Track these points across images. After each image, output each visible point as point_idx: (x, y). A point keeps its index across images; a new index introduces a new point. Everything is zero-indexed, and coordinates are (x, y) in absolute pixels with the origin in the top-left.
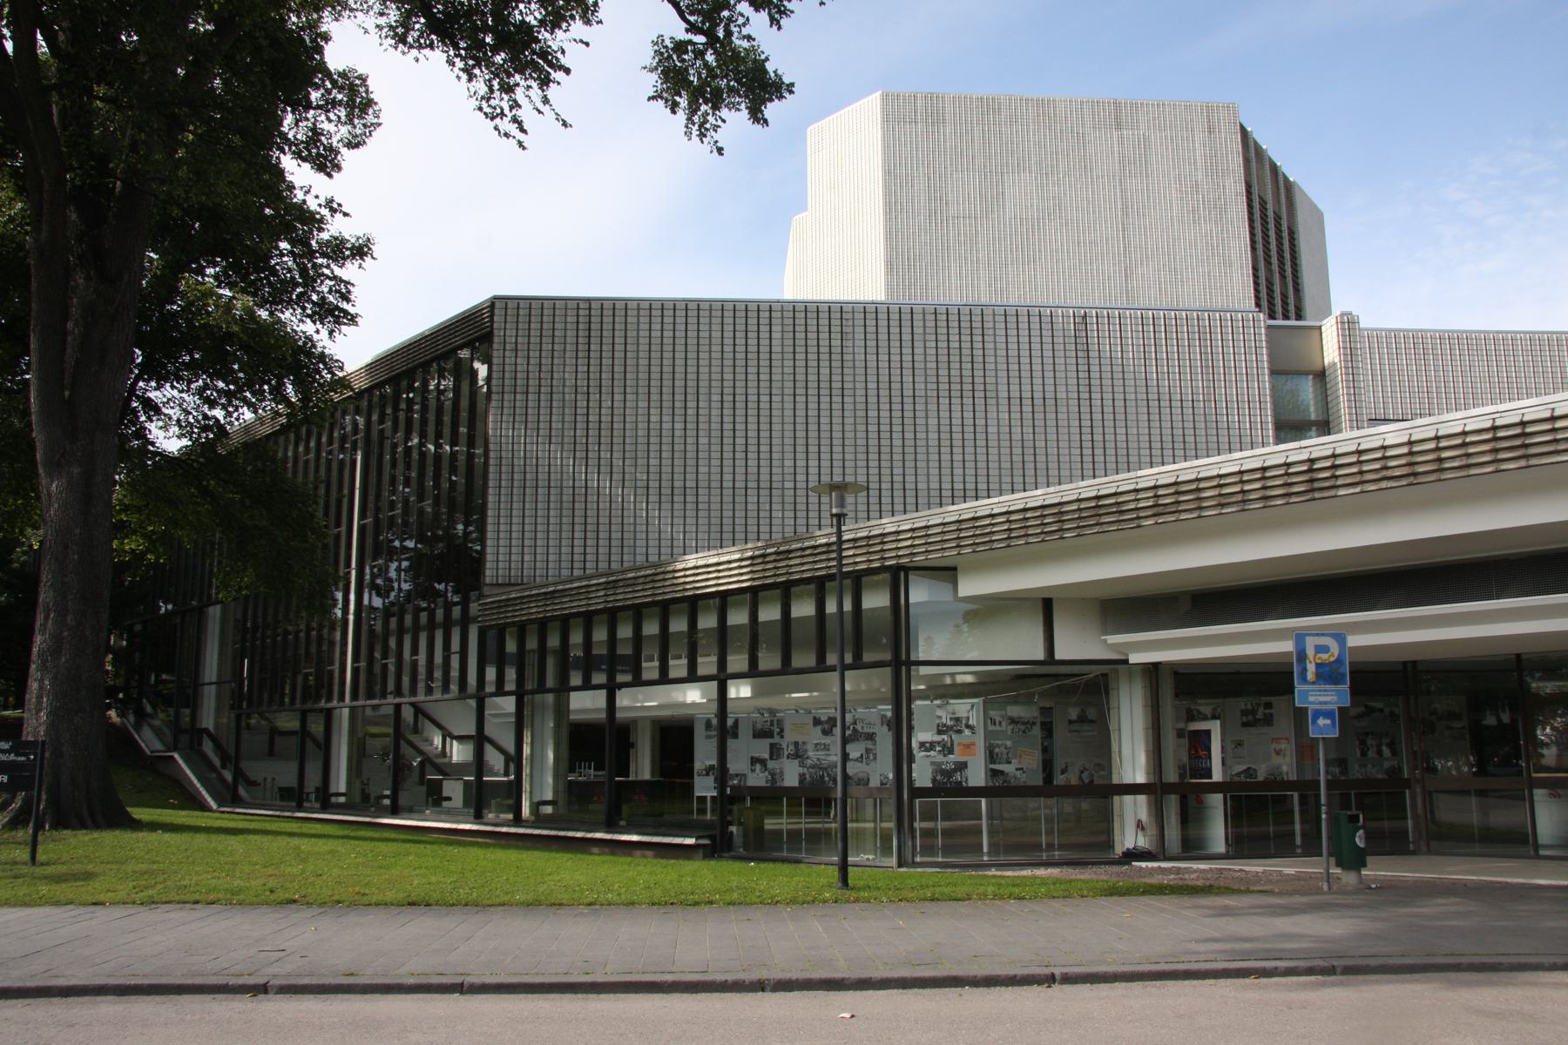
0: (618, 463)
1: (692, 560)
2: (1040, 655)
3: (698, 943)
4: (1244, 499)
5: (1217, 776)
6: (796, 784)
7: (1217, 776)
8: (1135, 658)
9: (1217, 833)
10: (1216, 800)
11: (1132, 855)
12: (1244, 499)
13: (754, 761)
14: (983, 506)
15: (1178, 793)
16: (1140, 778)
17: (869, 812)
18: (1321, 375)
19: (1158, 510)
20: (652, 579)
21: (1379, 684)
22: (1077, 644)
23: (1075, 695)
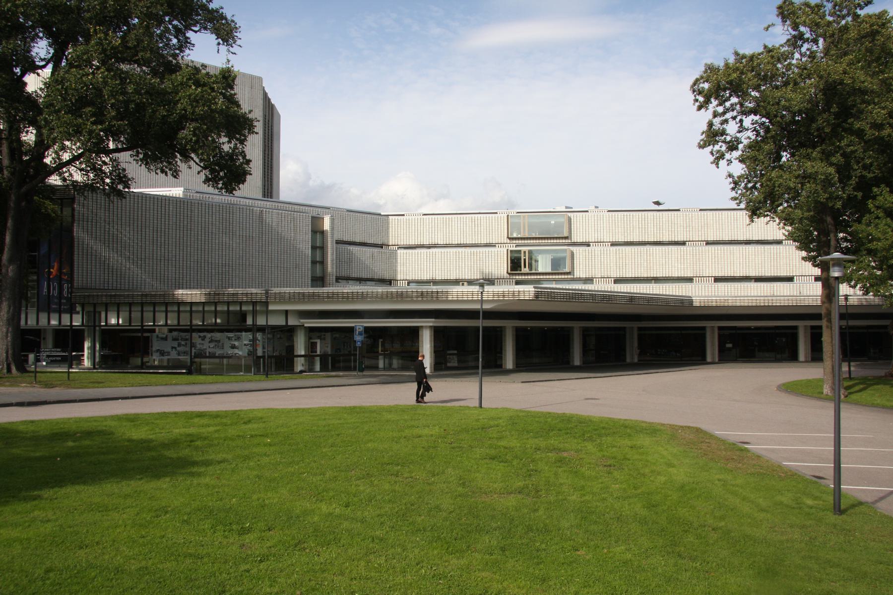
0: (119, 248)
1: (180, 292)
2: (284, 324)
3: (214, 388)
4: (348, 298)
5: (318, 353)
6: (819, 284)
7: (318, 353)
8: (306, 325)
9: (318, 367)
10: (318, 359)
11: (301, 372)
12: (348, 298)
13: (173, 348)
14: (283, 290)
15: (310, 357)
16: (303, 353)
17: (358, 338)
18: (323, 232)
19: (328, 297)
20: (164, 295)
21: (369, 332)
22: (292, 322)
23: (289, 332)
